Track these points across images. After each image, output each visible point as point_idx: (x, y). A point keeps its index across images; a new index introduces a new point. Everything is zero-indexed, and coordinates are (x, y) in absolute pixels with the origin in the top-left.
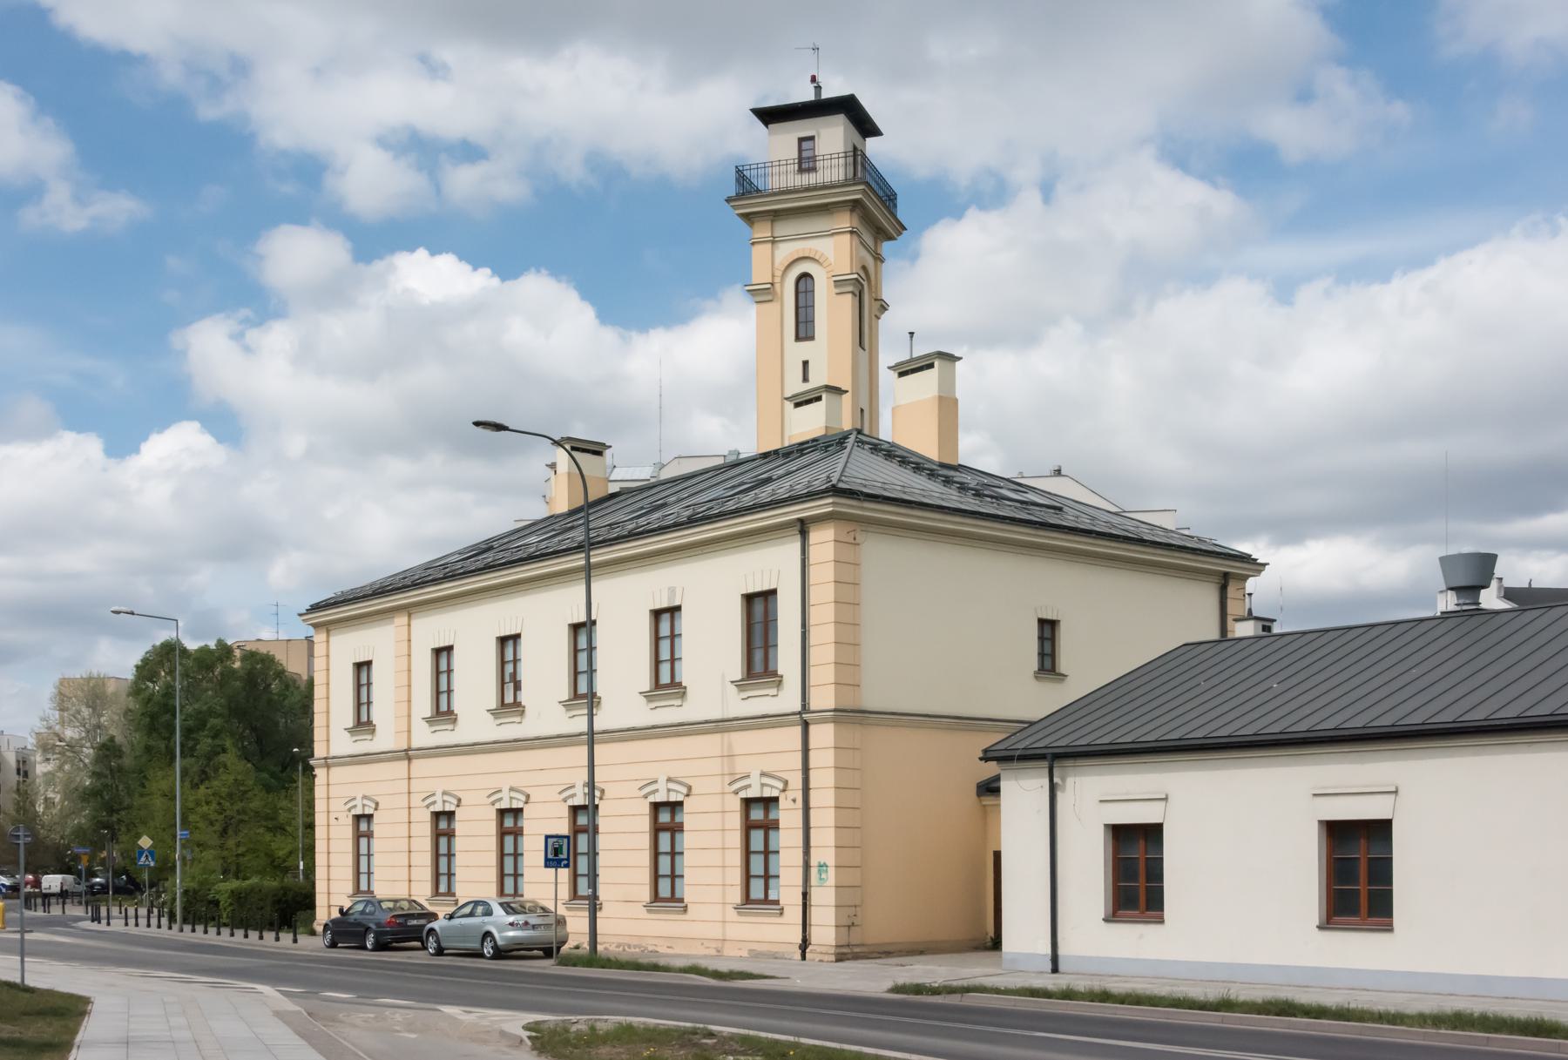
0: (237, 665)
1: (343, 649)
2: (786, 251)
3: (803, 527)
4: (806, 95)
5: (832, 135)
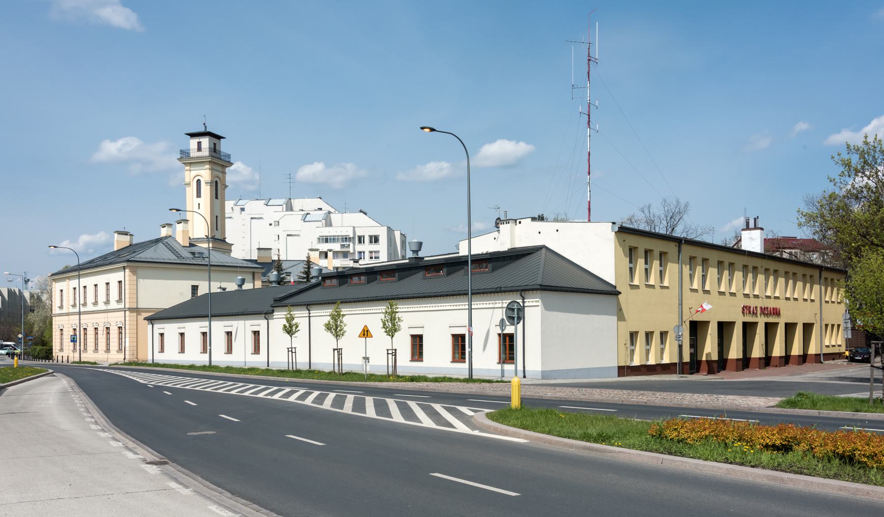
0: (211, 245)
1: (57, 286)
2: (193, 173)
3: (124, 268)
4: (202, 130)
5: (205, 142)
